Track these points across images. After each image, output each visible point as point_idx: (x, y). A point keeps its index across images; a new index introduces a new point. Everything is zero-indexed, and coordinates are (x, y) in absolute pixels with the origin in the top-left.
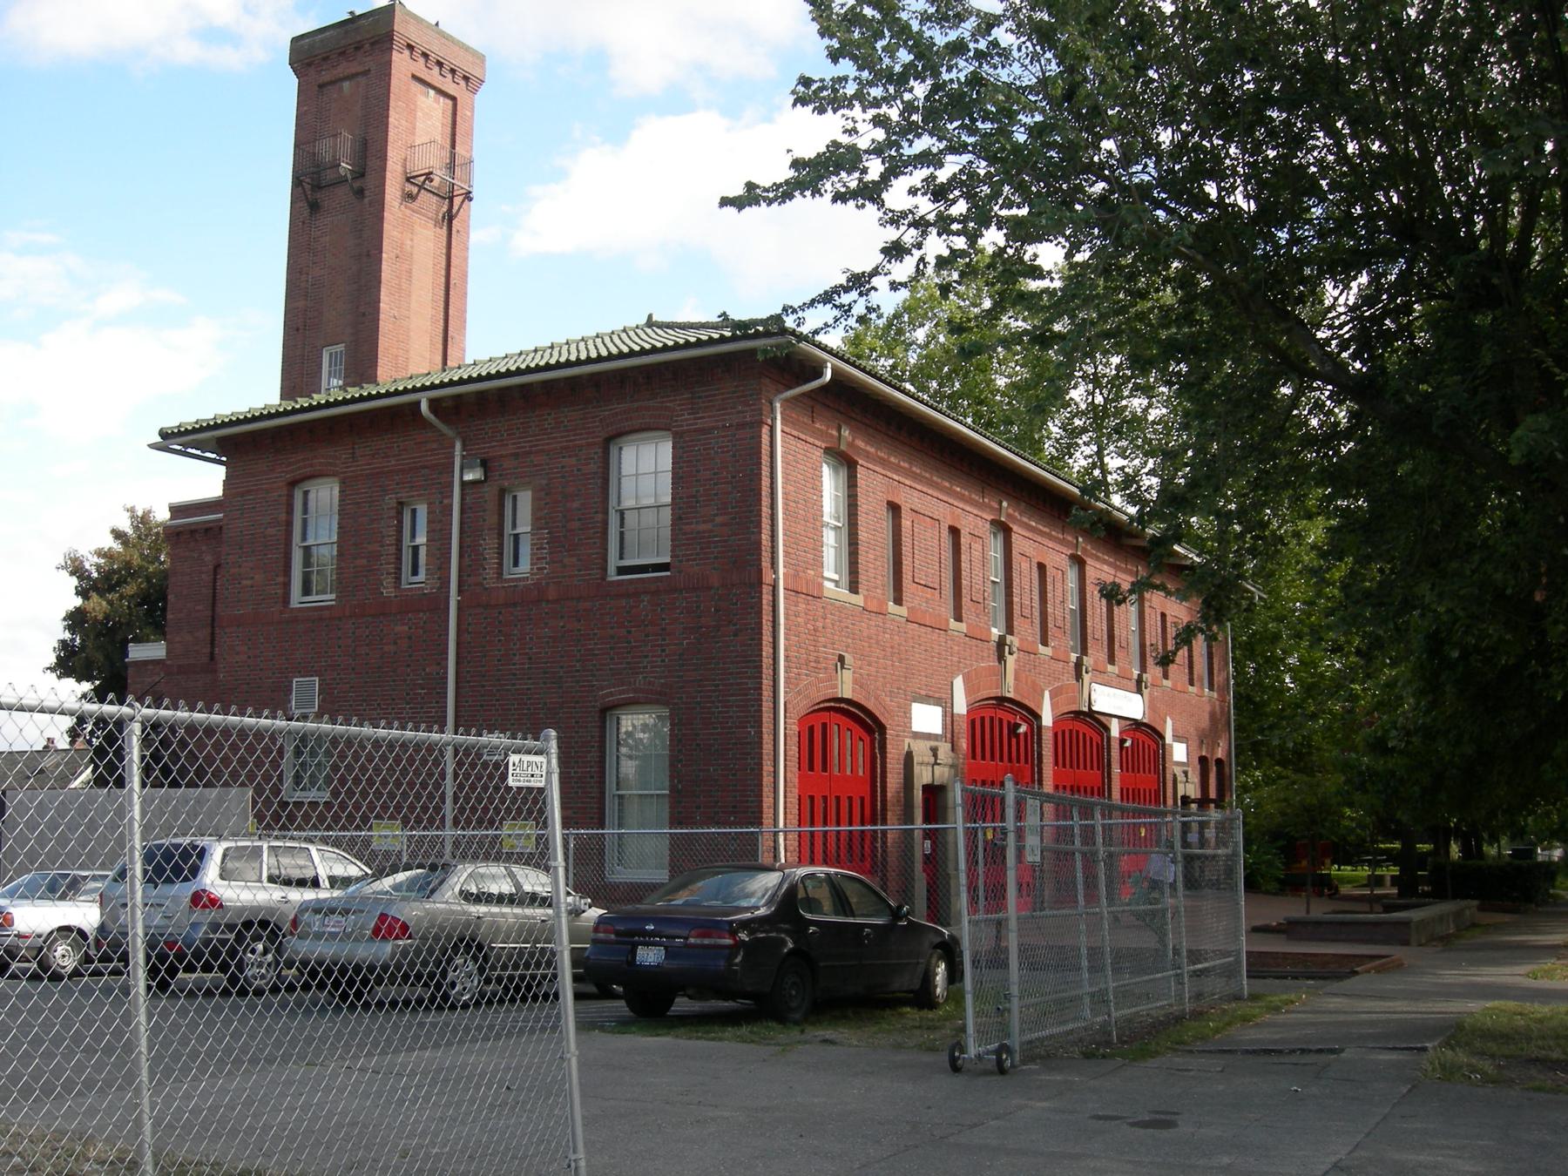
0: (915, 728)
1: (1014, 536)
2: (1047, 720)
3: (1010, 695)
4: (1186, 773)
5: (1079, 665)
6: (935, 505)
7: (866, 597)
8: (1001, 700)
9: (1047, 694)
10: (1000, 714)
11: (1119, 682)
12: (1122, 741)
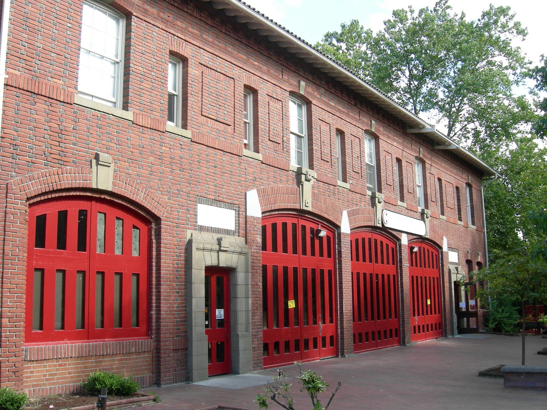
0: (200, 222)
1: (380, 141)
2: (345, 228)
3: (310, 209)
4: (457, 268)
5: (373, 197)
6: (331, 114)
7: (263, 155)
8: (301, 213)
9: (345, 213)
10: (302, 222)
11: (410, 211)
12: (412, 248)
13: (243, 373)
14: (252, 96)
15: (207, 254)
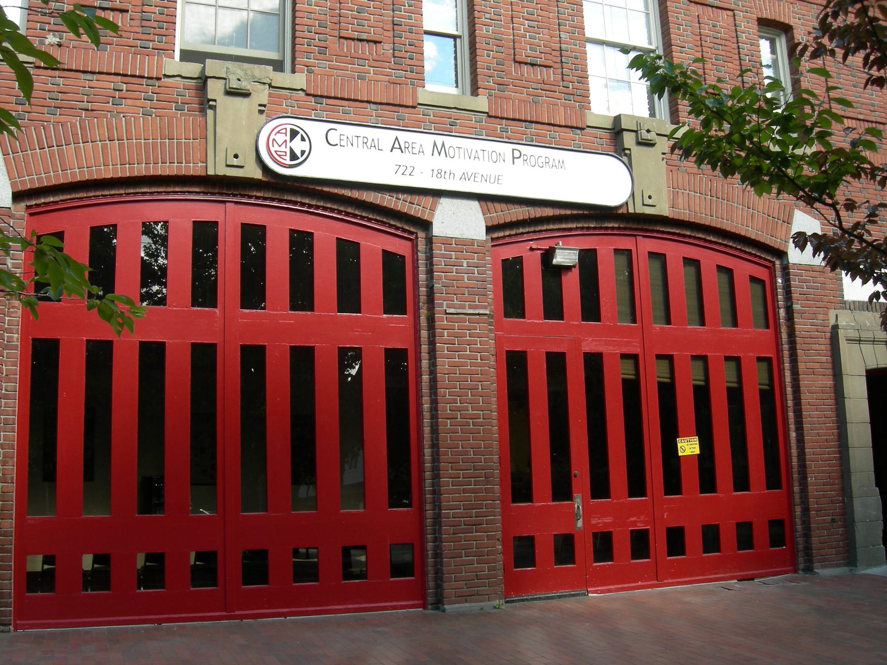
13: (870, 565)
14: (783, 40)
15: (867, 348)
